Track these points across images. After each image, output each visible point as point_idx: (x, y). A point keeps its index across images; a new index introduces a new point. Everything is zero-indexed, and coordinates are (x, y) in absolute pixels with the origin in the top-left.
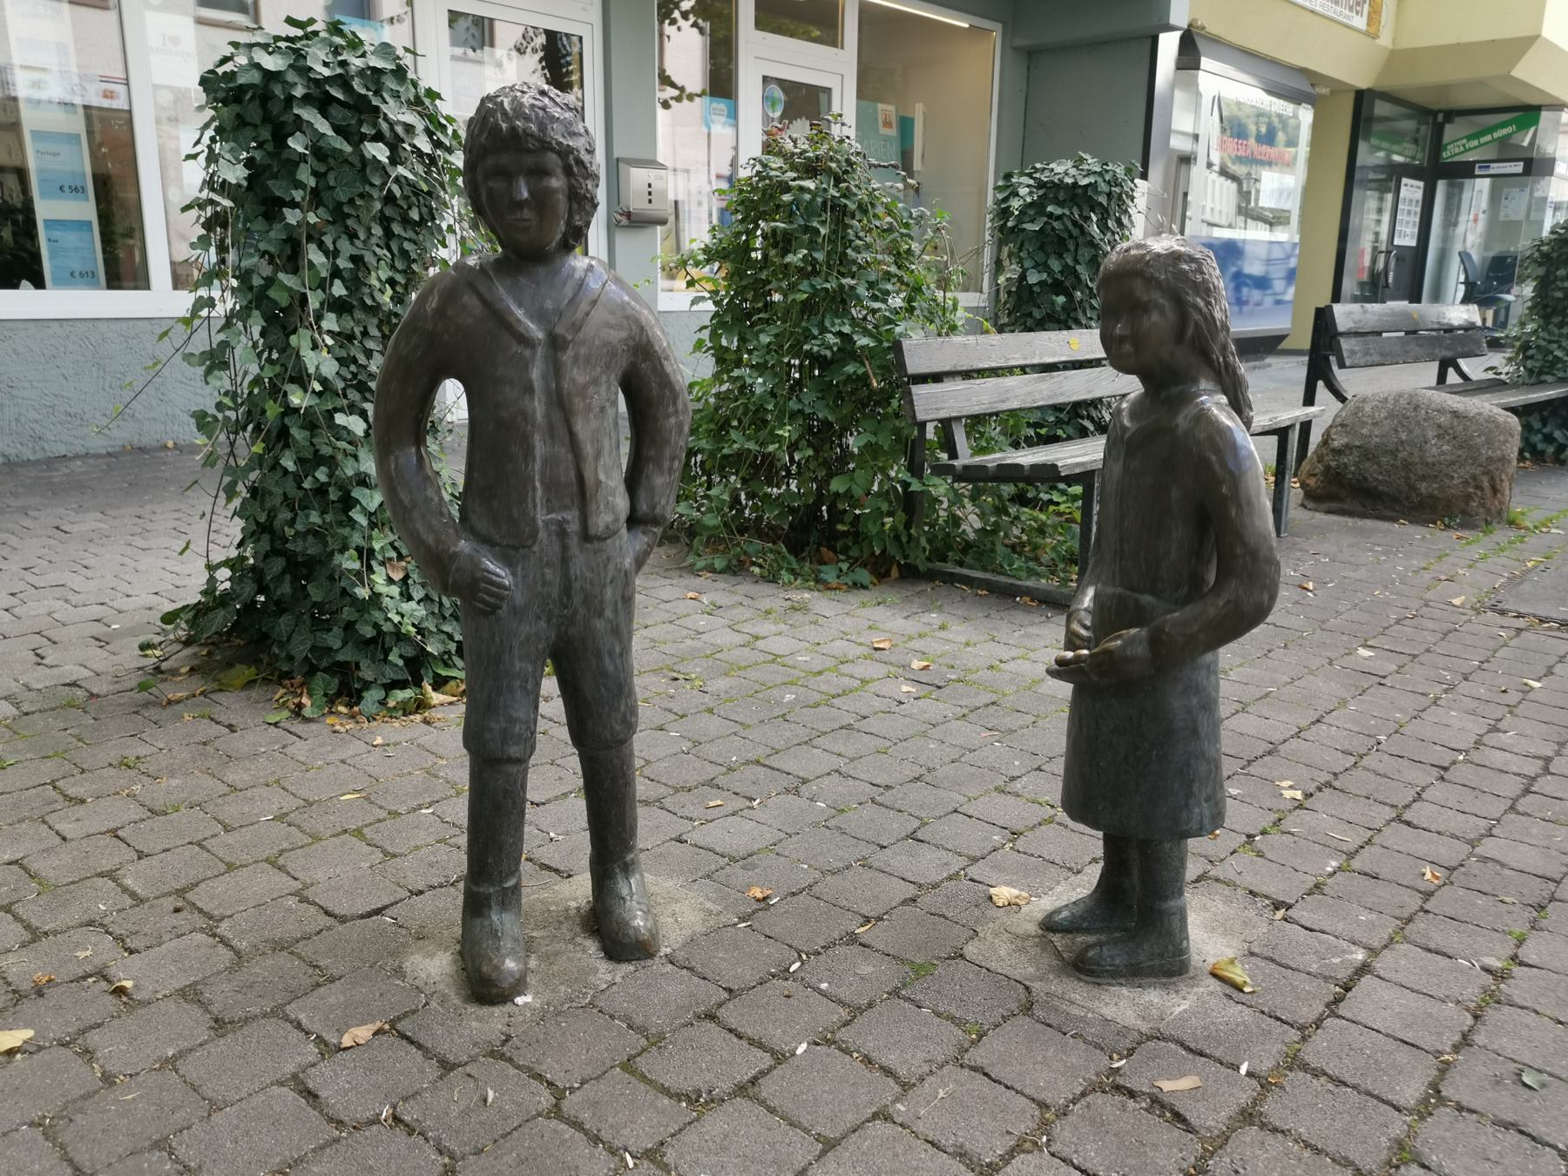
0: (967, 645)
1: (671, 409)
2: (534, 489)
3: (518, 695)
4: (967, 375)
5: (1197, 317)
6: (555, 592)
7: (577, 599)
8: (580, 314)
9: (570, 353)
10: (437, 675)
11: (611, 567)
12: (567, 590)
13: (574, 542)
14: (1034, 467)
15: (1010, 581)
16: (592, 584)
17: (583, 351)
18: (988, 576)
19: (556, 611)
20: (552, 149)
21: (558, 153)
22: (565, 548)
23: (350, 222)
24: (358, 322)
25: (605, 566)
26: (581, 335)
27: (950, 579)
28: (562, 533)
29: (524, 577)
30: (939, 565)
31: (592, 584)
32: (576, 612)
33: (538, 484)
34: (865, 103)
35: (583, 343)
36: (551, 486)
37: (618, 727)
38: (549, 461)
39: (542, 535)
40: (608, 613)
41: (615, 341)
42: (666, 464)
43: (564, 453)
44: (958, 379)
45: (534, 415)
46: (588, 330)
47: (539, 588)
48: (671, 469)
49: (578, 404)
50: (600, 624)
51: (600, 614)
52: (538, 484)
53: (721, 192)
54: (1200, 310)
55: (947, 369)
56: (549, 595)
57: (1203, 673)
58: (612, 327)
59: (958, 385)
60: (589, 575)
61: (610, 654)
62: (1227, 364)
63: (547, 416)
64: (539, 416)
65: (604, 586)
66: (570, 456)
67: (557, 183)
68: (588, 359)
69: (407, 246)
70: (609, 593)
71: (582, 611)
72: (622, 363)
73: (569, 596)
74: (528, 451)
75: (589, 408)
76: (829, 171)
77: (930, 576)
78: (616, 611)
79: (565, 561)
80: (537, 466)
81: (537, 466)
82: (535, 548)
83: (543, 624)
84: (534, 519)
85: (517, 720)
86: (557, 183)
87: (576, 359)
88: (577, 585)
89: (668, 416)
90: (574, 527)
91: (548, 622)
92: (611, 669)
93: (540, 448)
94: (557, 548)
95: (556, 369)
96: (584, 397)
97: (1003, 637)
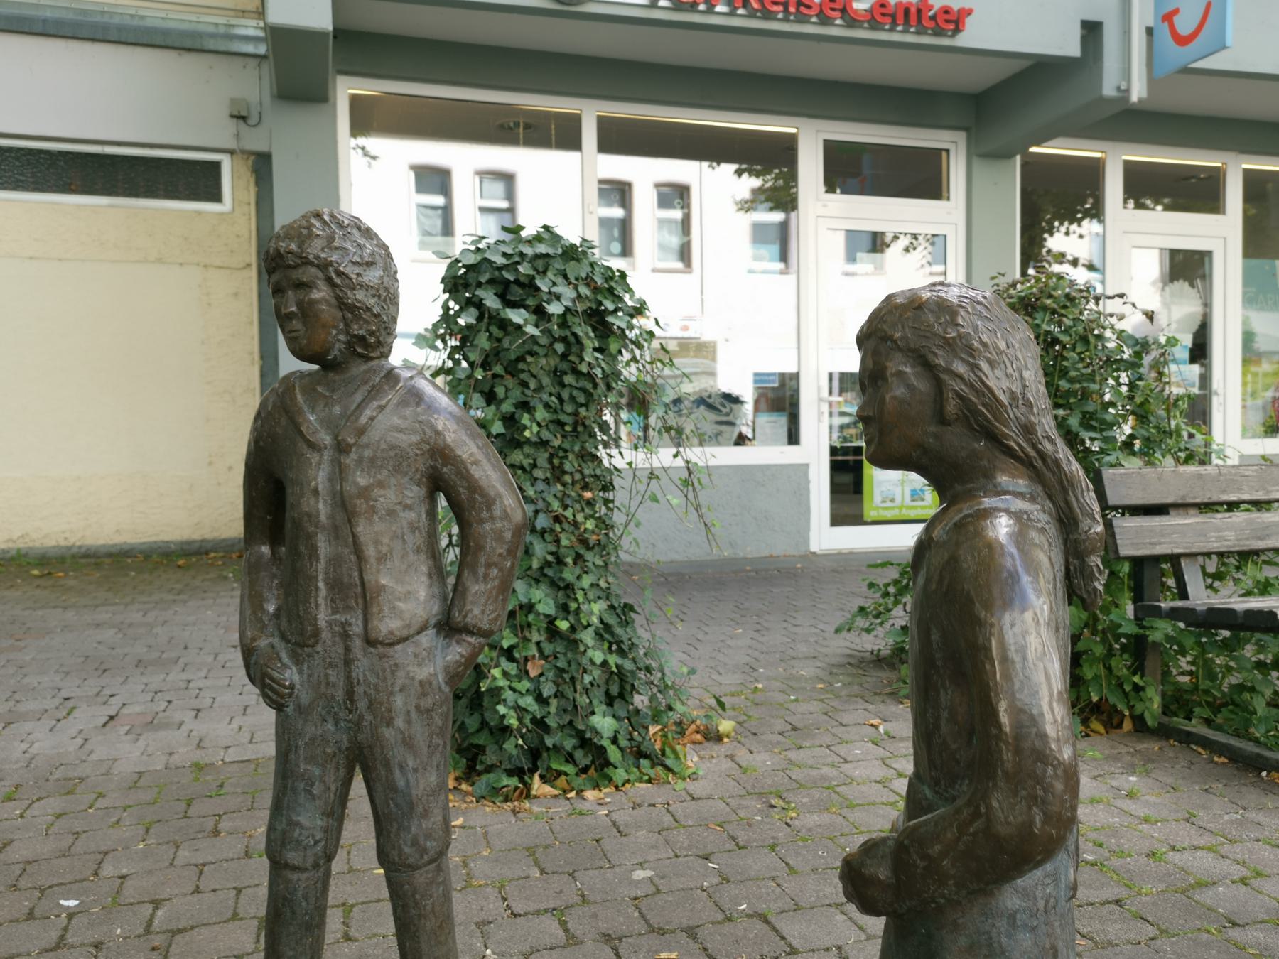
0: (1146, 820)
1: (485, 515)
2: (317, 589)
3: (302, 797)
4: (1207, 507)
5: (957, 386)
6: (340, 695)
7: (362, 704)
8: (363, 420)
9: (353, 456)
10: (549, 769)
11: (401, 674)
12: (350, 694)
13: (357, 644)
14: (1249, 613)
15: (1257, 750)
16: (377, 691)
17: (367, 453)
18: (1234, 742)
19: (342, 715)
20: (311, 264)
21: (317, 266)
22: (348, 649)
23: (523, 376)
24: (527, 456)
25: (393, 673)
26: (364, 439)
27: (1187, 739)
28: (345, 636)
29: (309, 676)
30: (1179, 722)
31: (377, 691)
32: (361, 717)
33: (321, 585)
34: (1254, 262)
35: (367, 446)
36: (337, 586)
37: (407, 850)
38: (335, 562)
39: (325, 635)
40: (399, 722)
41: (404, 445)
42: (481, 571)
43: (347, 552)
44: (1192, 511)
45: (318, 515)
46: (374, 435)
47: (323, 689)
48: (486, 576)
49: (361, 505)
50: (388, 733)
51: (389, 723)
52: (321, 585)
53: (640, 310)
54: (961, 377)
55: (1170, 500)
56: (333, 697)
57: (1002, 924)
58: (401, 431)
59: (1192, 520)
60: (373, 680)
61: (401, 767)
62: (1042, 455)
63: (331, 517)
64: (323, 518)
65: (392, 693)
66: (353, 558)
67: (321, 293)
68: (372, 460)
69: (575, 393)
70: (399, 701)
71: (368, 717)
72: (422, 465)
73: (352, 701)
74: (314, 549)
75: (373, 510)
76: (1045, 309)
77: (1164, 732)
78: (409, 722)
79: (348, 663)
80: (321, 566)
81: (321, 566)
82: (319, 648)
83: (330, 727)
84: (315, 619)
85: (298, 824)
86: (321, 293)
87: (360, 461)
88: (359, 690)
89: (482, 521)
90: (357, 628)
91: (336, 724)
92: (401, 783)
93: (324, 547)
94: (340, 650)
95: (339, 472)
96: (367, 499)
97: (1203, 816)
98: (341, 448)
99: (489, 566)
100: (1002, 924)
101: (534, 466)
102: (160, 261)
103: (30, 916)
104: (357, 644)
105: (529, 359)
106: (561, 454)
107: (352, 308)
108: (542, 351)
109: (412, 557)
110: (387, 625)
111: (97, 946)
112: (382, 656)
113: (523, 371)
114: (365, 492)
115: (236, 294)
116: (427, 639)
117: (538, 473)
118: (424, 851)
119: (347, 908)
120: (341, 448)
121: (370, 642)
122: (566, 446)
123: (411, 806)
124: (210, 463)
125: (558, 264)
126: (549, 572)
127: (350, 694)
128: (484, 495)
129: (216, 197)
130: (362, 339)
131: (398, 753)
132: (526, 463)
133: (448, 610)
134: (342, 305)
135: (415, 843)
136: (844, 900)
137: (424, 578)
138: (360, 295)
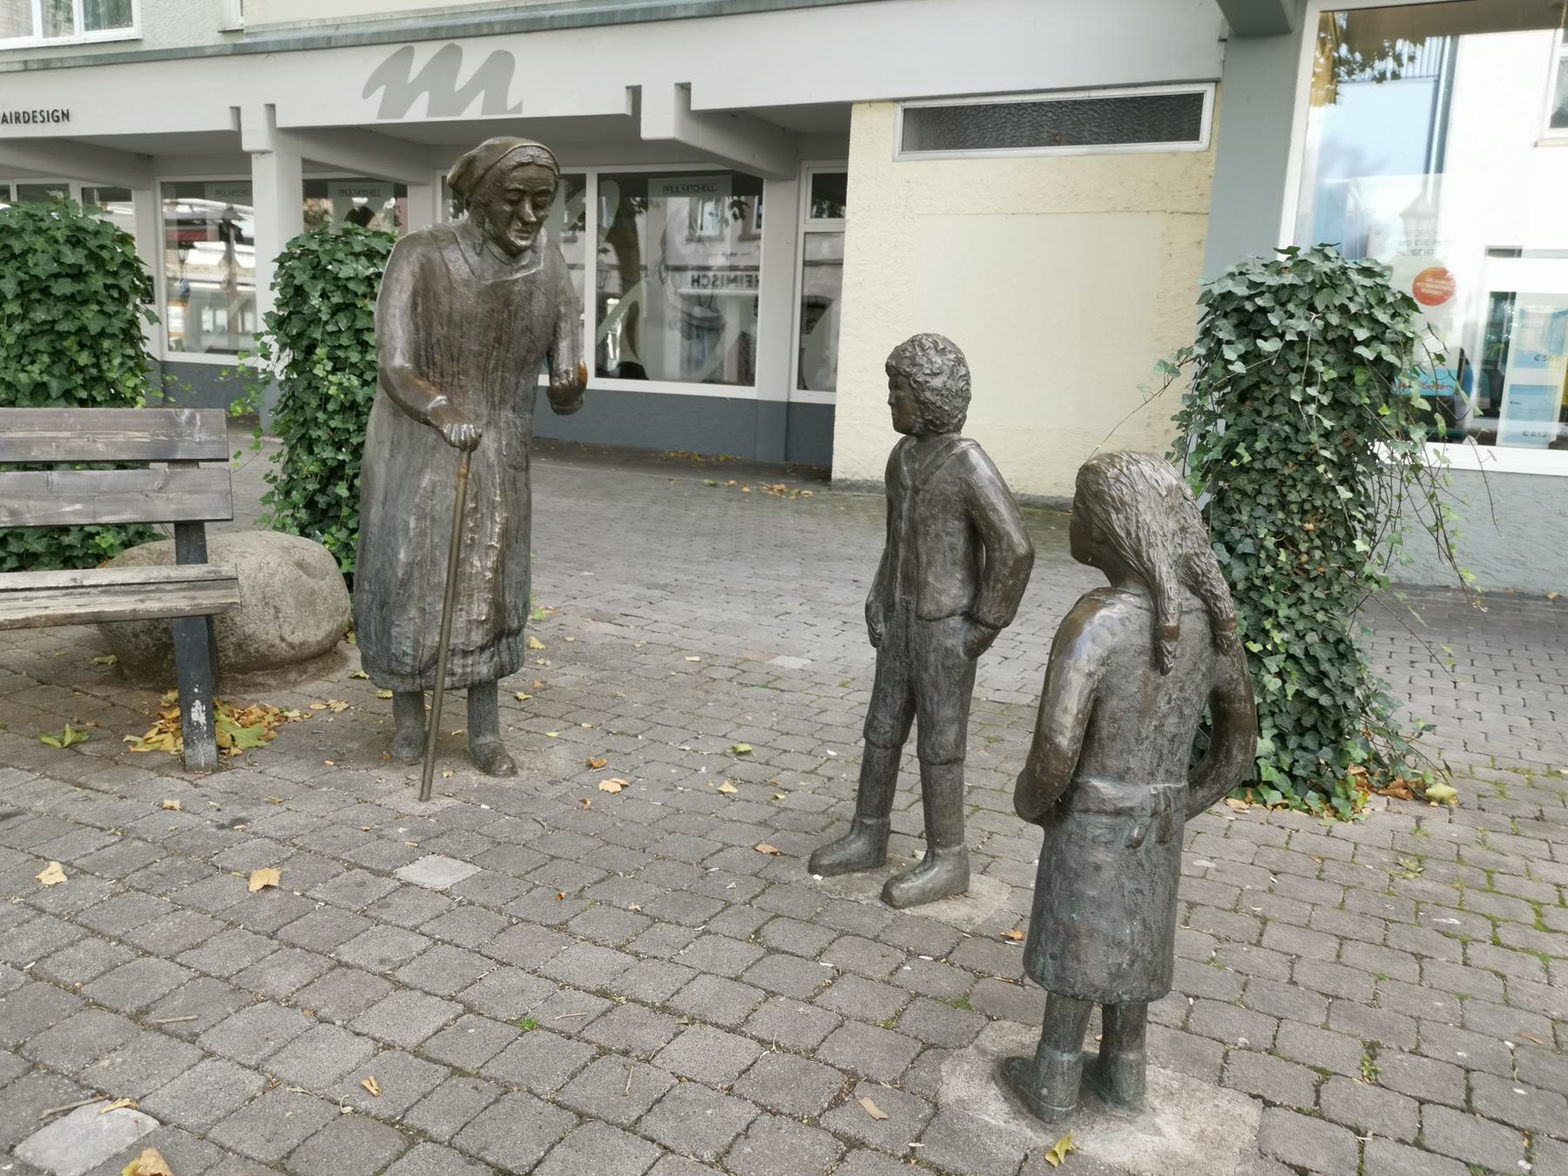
7: (913, 654)
11: (934, 640)
12: (907, 646)
28: (907, 610)
38: (907, 562)
39: (898, 607)
40: (931, 671)
49: (921, 529)
50: (925, 676)
70: (932, 657)
72: (960, 508)
75: (927, 533)
79: (907, 626)
88: (912, 645)
98: (916, 491)
99: (996, 581)
100: (1065, 837)
101: (1259, 492)
102: (1128, 209)
103: (810, 753)
104: (913, 615)
105: (1264, 387)
106: (1290, 482)
107: (923, 403)
108: (1276, 381)
109: (949, 566)
110: (928, 607)
111: (830, 779)
112: (925, 627)
113: (1257, 399)
114: (924, 521)
115: (1199, 243)
116: (956, 622)
117: (1263, 500)
118: (938, 755)
119: (1191, 905)
120: (916, 491)
121: (919, 617)
122: (1297, 475)
123: (933, 725)
124: (1149, 425)
125: (1303, 295)
126: (1253, 594)
127: (907, 646)
128: (997, 532)
129: (1194, 135)
130: (931, 422)
131: (929, 690)
132: (1249, 488)
133: (971, 607)
134: (918, 401)
135: (932, 748)
136: (1012, 808)
137: (959, 584)
138: (928, 394)
